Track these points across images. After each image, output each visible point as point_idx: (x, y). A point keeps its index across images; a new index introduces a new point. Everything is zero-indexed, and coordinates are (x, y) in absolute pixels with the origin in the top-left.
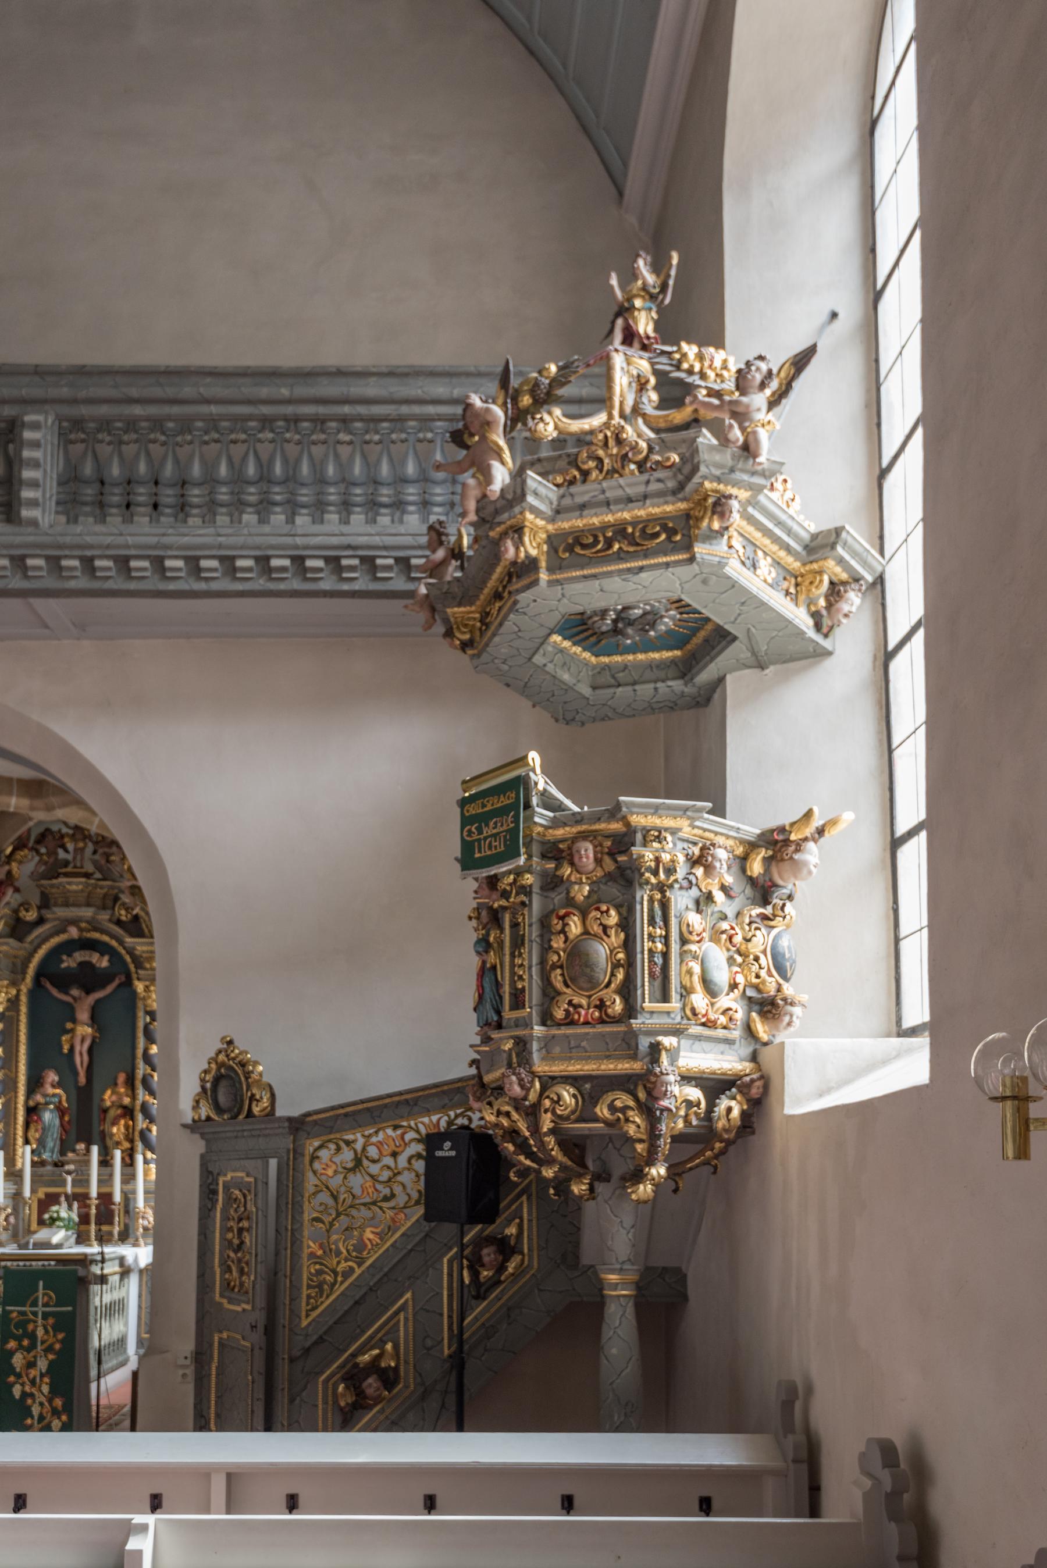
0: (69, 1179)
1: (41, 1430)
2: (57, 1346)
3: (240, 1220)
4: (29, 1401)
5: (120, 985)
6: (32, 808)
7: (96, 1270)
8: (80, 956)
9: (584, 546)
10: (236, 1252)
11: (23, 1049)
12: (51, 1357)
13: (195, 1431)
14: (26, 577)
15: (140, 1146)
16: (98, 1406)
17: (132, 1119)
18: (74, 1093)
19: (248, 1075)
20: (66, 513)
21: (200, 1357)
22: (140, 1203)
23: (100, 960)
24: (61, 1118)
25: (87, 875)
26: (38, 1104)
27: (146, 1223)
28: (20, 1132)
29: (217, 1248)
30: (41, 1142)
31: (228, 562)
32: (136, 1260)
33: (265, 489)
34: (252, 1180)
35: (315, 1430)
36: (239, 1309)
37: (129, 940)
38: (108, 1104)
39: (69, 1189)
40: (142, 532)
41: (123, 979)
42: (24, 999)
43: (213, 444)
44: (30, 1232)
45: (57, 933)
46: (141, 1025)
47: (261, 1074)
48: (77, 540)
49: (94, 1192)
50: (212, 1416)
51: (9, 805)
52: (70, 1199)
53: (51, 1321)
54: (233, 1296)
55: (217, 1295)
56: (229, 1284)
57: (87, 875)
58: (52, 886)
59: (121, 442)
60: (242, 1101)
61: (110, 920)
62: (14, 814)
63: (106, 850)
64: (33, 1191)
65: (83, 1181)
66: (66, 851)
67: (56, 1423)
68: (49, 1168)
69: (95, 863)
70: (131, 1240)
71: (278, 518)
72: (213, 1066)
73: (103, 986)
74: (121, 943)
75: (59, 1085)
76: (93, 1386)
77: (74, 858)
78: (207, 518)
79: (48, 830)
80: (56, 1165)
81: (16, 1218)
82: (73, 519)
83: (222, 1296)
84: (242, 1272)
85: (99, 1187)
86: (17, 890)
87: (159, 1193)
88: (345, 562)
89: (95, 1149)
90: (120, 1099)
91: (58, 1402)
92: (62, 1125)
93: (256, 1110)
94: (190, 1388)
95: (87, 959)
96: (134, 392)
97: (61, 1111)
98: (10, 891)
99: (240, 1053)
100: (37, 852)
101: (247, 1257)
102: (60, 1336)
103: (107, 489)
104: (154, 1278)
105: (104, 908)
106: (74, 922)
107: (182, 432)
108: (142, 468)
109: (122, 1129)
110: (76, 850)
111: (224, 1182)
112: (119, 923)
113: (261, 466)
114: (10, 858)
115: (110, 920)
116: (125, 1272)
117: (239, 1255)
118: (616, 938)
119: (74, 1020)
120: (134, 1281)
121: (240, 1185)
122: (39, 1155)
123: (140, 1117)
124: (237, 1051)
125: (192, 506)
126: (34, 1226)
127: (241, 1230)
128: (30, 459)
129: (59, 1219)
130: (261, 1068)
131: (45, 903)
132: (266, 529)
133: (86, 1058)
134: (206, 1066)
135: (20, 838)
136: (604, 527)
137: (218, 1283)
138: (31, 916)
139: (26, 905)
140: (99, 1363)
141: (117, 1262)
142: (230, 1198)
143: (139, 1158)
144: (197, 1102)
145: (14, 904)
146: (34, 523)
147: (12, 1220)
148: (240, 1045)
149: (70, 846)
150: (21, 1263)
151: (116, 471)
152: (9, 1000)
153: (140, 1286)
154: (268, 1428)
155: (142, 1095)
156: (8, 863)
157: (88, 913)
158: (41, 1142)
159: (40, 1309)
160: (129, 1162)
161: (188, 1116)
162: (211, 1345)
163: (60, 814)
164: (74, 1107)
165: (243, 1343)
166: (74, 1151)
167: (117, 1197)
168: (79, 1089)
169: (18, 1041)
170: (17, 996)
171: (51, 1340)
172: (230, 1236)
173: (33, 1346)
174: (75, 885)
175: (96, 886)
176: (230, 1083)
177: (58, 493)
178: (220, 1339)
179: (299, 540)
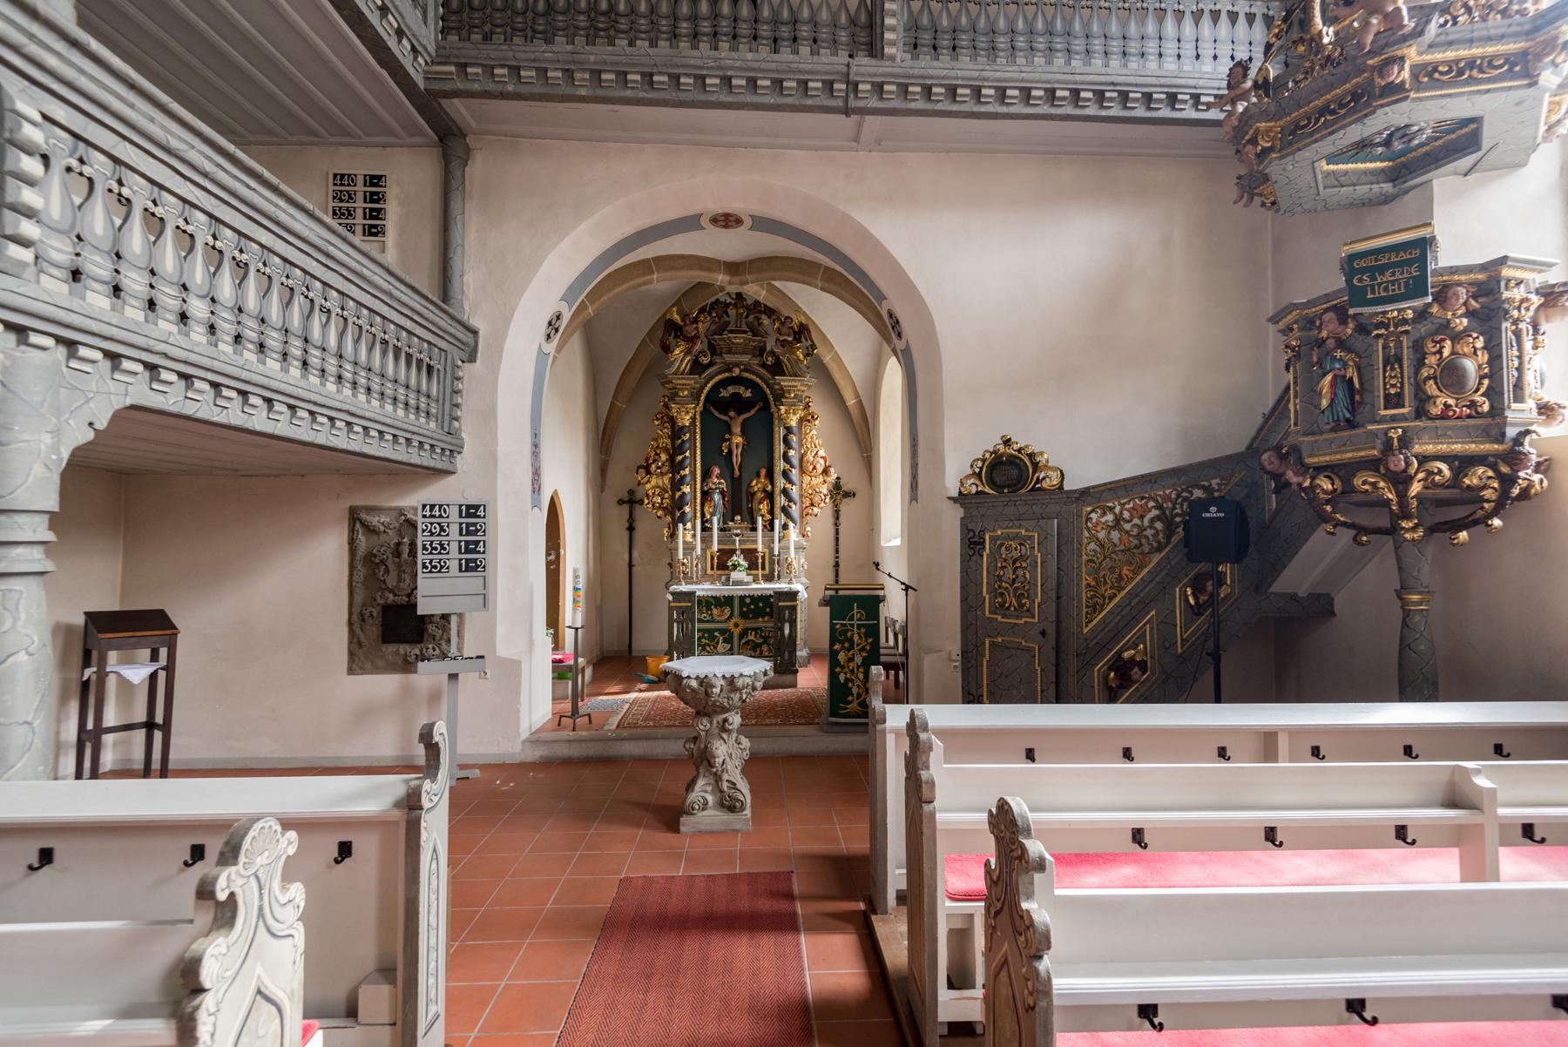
6: (730, 283)
8: (731, 390)
9: (1442, 73)
14: (881, 98)
31: (1026, 93)
40: (965, 68)
48: (922, 72)
71: (1059, 61)
82: (915, 58)
88: (1108, 95)
97: (722, 493)
103: (939, 35)
106: (737, 365)
108: (964, 20)
112: (764, 365)
118: (1483, 357)
136: (1457, 61)
138: (705, 361)
146: (892, 58)
151: (945, 22)
154: (1218, 700)
157: (745, 358)
159: (855, 622)
174: (738, 339)
179: (1078, 78)
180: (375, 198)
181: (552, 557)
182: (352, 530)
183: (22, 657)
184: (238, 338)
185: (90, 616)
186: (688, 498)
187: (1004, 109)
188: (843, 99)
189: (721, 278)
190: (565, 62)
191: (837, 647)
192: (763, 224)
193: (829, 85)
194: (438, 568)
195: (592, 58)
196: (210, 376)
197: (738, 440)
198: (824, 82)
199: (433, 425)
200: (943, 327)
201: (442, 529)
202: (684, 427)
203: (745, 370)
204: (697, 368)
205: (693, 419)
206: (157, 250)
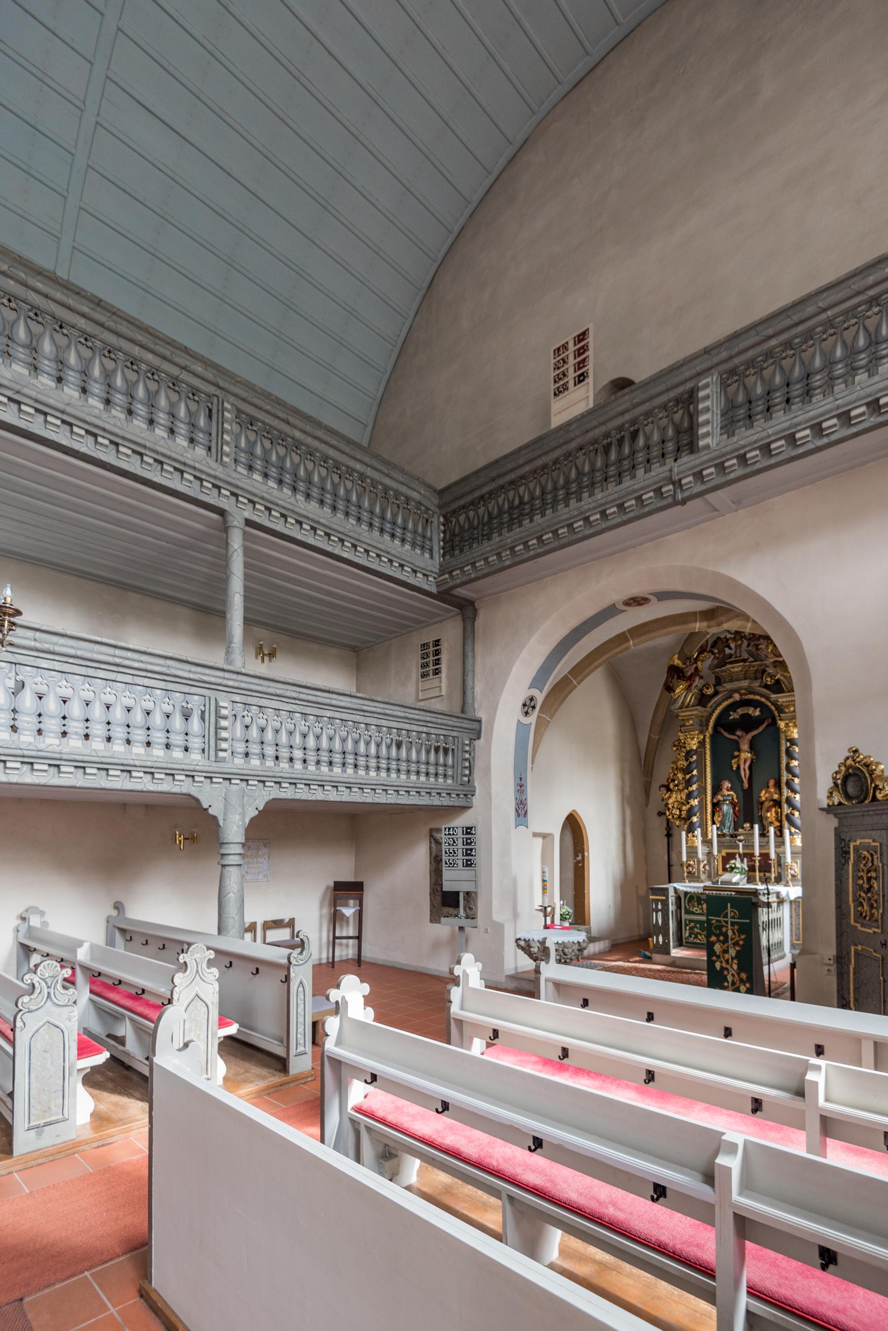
0: (741, 844)
1: (734, 990)
2: (741, 942)
3: (869, 871)
4: (726, 973)
5: (768, 726)
6: (709, 627)
7: (764, 899)
8: (741, 711)
10: (866, 893)
11: (708, 770)
12: (737, 948)
13: (838, 1007)
14: (703, 482)
15: (786, 824)
16: (769, 981)
17: (780, 807)
18: (741, 793)
19: (871, 773)
20: (727, 433)
21: (841, 960)
22: (789, 859)
23: (754, 712)
24: (734, 808)
25: (744, 661)
26: (719, 801)
27: (793, 872)
28: (709, 817)
29: (851, 889)
30: (722, 823)
32: (788, 894)
33: (873, 350)
34: (878, 844)
35: (880, 1014)
36: (870, 931)
37: (773, 696)
38: (764, 799)
39: (741, 851)
41: (770, 721)
42: (708, 740)
43: (830, 338)
44: (718, 875)
45: (726, 699)
46: (783, 749)
47: (882, 771)
48: (736, 446)
49: (757, 853)
50: (852, 1000)
51: (695, 628)
52: (742, 857)
53: (736, 927)
54: (865, 922)
55: (852, 921)
56: (861, 914)
57: (744, 661)
58: (722, 671)
59: (762, 369)
60: (867, 791)
61: (760, 686)
62: (698, 633)
63: (756, 642)
64: (719, 851)
65: (749, 845)
66: (730, 648)
67: (743, 988)
68: (728, 838)
69: (749, 652)
70: (783, 882)
72: (843, 768)
73: (757, 728)
74: (768, 698)
75: (731, 789)
76: (766, 968)
77: (736, 652)
78: (827, 393)
79: (719, 638)
80: (732, 836)
81: (710, 867)
83: (855, 921)
84: (871, 907)
85: (760, 849)
86: (701, 677)
87: (806, 854)
89: (756, 827)
90: (772, 795)
91: (744, 976)
92: (734, 813)
93: (879, 796)
94: (834, 979)
95: (746, 712)
96: (770, 331)
97: (733, 805)
98: (697, 679)
99: (865, 758)
100: (713, 653)
101: (876, 897)
102: (743, 937)
104: (805, 908)
105: (756, 679)
106: (737, 691)
107: (806, 341)
109: (774, 815)
110: (736, 647)
111: (854, 846)
112: (766, 686)
113: (870, 335)
114: (696, 660)
115: (760, 686)
116: (781, 902)
117: (869, 895)
119: (739, 750)
120: (786, 907)
121: (867, 848)
122: (722, 830)
123: (785, 806)
124: (861, 757)
125: (814, 389)
126: (720, 872)
127: (869, 879)
128: (703, 409)
129: (736, 868)
130: (882, 767)
131: (719, 682)
132: (876, 378)
133: (748, 772)
134: (837, 769)
135: (702, 646)
137: (852, 913)
138: (710, 691)
139: (707, 686)
140: (769, 955)
141: (775, 895)
142: (859, 857)
143: (787, 832)
144: (831, 793)
145: (700, 686)
146: (707, 447)
147: (707, 867)
148: (864, 752)
149: (733, 645)
150: (714, 892)
152: (699, 742)
153: (791, 911)
154: (884, 1014)
155: (786, 792)
156: (696, 663)
157: (745, 683)
158: (722, 823)
159: (729, 920)
160: (780, 833)
161: (825, 803)
162: (849, 953)
163: (726, 626)
164: (742, 800)
165: (874, 954)
166: (743, 828)
167: (773, 856)
168: (744, 791)
169: (705, 765)
170: (704, 738)
171: (737, 939)
172: (861, 882)
173: (725, 941)
174: (737, 668)
175: (750, 666)
176: (856, 780)
177: (722, 422)
178: (856, 950)
180: (437, 653)
181: (579, 858)
182: (430, 842)
183: (232, 894)
184: (318, 762)
185: (335, 883)
186: (696, 809)
187: (825, 440)
188: (672, 495)
189: (698, 626)
190: (497, 549)
191: (713, 938)
192: (663, 596)
193: (658, 491)
194: (452, 865)
195: (509, 540)
196: (303, 782)
197: (746, 755)
198: (654, 491)
199: (449, 781)
200: (810, 647)
201: (454, 842)
202: (692, 750)
203: (750, 693)
204: (703, 700)
205: (702, 744)
206: (278, 736)
